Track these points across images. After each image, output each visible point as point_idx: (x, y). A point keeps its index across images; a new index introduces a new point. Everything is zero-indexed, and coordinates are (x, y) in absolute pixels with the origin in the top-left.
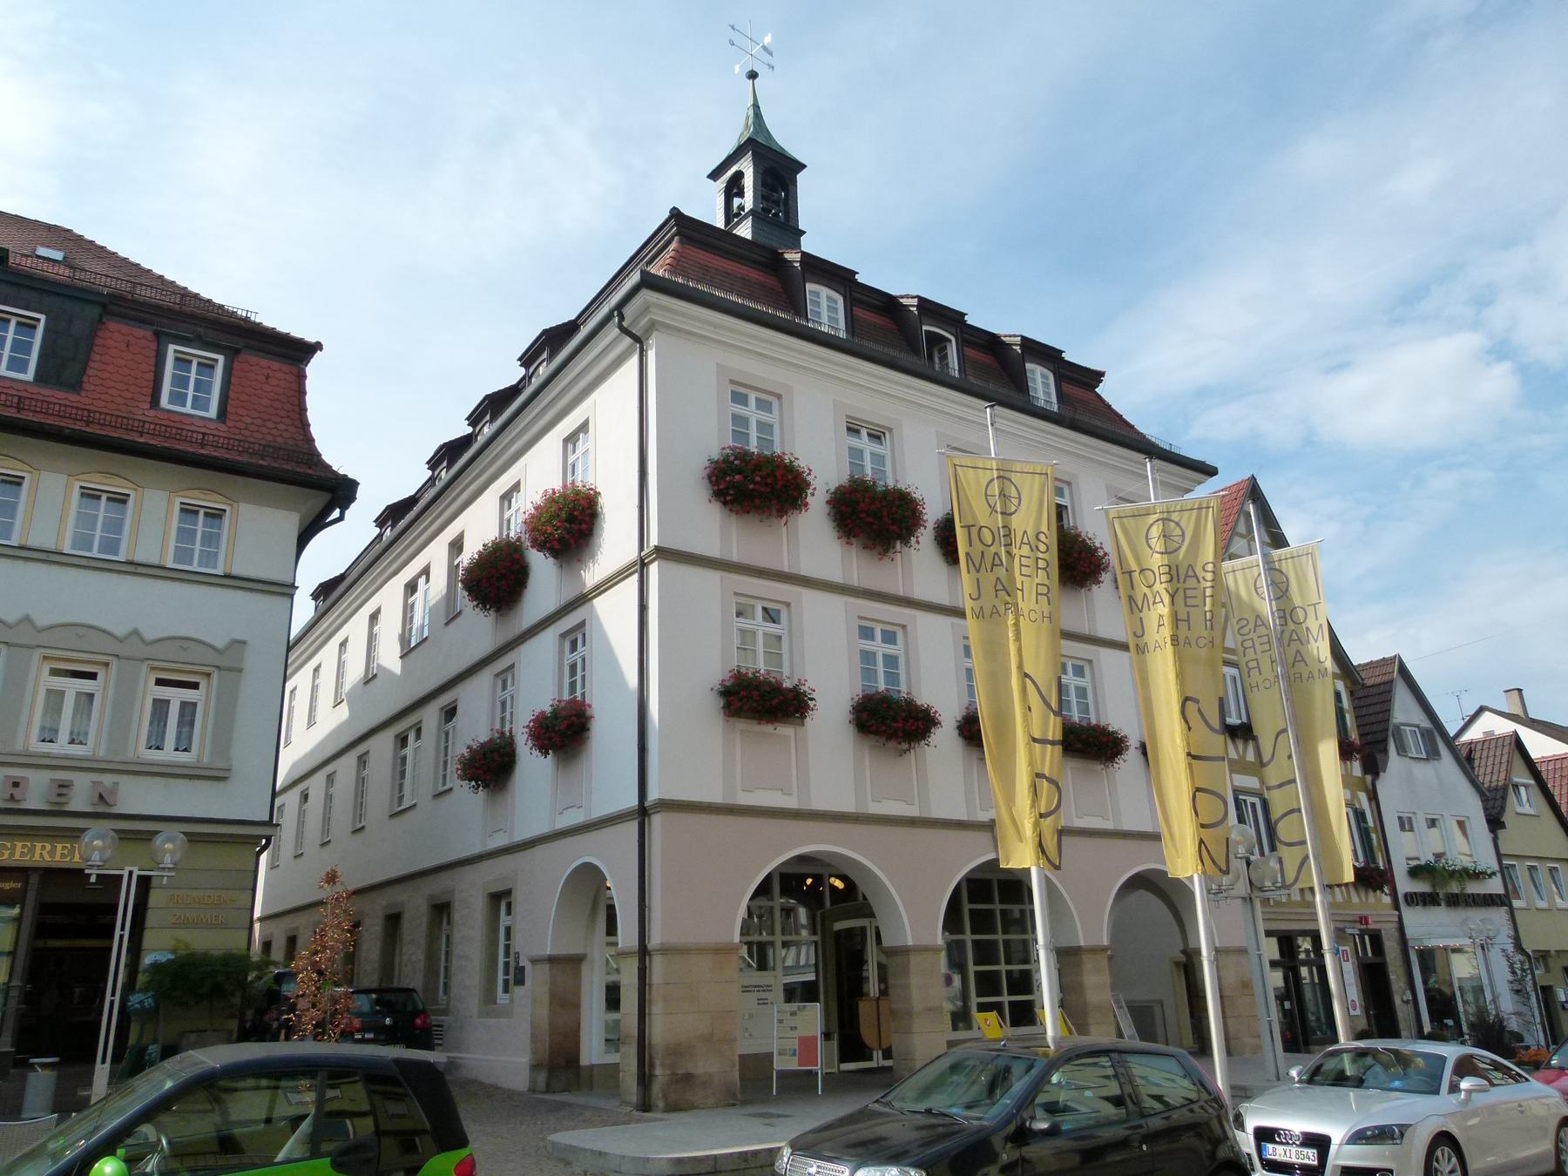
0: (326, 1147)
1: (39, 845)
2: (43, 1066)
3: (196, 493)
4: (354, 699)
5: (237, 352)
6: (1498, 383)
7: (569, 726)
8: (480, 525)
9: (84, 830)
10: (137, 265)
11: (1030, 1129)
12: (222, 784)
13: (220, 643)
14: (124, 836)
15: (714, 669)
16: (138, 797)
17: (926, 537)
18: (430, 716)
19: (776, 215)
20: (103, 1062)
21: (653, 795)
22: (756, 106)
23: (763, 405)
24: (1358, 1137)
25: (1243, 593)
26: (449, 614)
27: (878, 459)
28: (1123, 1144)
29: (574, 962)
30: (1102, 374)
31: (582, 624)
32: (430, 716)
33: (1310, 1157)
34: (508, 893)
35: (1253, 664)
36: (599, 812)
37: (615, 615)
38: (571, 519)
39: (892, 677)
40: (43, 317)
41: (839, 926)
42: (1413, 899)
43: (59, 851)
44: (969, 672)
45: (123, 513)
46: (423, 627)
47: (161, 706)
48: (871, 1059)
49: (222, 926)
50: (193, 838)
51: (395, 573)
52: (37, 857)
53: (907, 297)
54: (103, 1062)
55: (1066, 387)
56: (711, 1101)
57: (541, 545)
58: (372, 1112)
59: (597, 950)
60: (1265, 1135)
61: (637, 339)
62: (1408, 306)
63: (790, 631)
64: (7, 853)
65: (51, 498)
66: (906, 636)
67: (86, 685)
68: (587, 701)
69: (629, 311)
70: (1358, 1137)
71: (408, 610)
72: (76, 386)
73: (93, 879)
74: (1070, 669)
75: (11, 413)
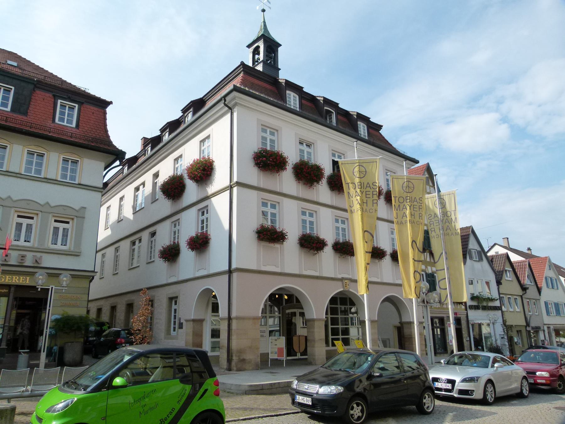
0: (177, 376)
1: (14, 277)
2: (24, 352)
3: (68, 154)
4: (113, 227)
5: (82, 103)
6: (503, 131)
7: (202, 242)
8: (166, 169)
9: (61, 274)
10: (42, 69)
11: (373, 375)
12: (77, 257)
13: (77, 208)
14: (50, 275)
15: (255, 223)
16: (49, 261)
17: (324, 181)
18: (145, 235)
19: (270, 62)
20: (44, 352)
21: (234, 266)
22: (264, 22)
23: (272, 134)
24: (464, 380)
25: (431, 206)
26: (153, 199)
27: (309, 154)
28: (399, 380)
29: (201, 321)
30: (382, 126)
31: (207, 206)
32: (145, 235)
33: (449, 386)
34: (177, 297)
35: (433, 230)
36: (212, 271)
37: (220, 205)
38: (204, 170)
39: (312, 229)
40: (13, 88)
41: (288, 311)
42: (471, 307)
43: (21, 279)
44: (393, 239)
45: (5, 153)
46: (142, 203)
47: (56, 229)
48: (296, 356)
49: (78, 307)
50: (73, 276)
51: (131, 183)
52: (14, 281)
53: (319, 97)
54: (44, 352)
55: (370, 130)
56: (251, 368)
57: (191, 178)
58: (189, 366)
59: (209, 317)
60: (435, 380)
61: (230, 108)
62: (474, 102)
63: (279, 212)
64: (3, 280)
65: (17, 153)
66: (316, 215)
67: (66, 226)
68: (209, 233)
69: (228, 99)
70: (464, 380)
71: (136, 197)
72: (26, 113)
73: (39, 290)
74: (340, 221)
75: (3, 123)
